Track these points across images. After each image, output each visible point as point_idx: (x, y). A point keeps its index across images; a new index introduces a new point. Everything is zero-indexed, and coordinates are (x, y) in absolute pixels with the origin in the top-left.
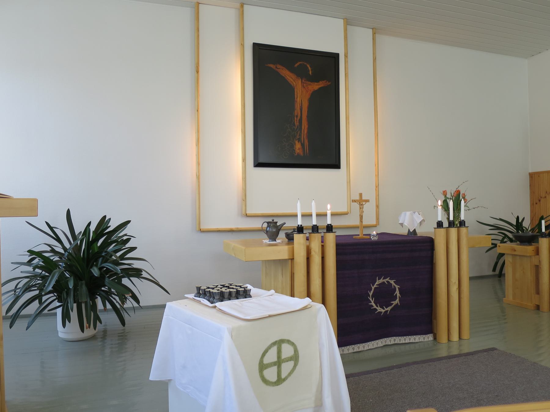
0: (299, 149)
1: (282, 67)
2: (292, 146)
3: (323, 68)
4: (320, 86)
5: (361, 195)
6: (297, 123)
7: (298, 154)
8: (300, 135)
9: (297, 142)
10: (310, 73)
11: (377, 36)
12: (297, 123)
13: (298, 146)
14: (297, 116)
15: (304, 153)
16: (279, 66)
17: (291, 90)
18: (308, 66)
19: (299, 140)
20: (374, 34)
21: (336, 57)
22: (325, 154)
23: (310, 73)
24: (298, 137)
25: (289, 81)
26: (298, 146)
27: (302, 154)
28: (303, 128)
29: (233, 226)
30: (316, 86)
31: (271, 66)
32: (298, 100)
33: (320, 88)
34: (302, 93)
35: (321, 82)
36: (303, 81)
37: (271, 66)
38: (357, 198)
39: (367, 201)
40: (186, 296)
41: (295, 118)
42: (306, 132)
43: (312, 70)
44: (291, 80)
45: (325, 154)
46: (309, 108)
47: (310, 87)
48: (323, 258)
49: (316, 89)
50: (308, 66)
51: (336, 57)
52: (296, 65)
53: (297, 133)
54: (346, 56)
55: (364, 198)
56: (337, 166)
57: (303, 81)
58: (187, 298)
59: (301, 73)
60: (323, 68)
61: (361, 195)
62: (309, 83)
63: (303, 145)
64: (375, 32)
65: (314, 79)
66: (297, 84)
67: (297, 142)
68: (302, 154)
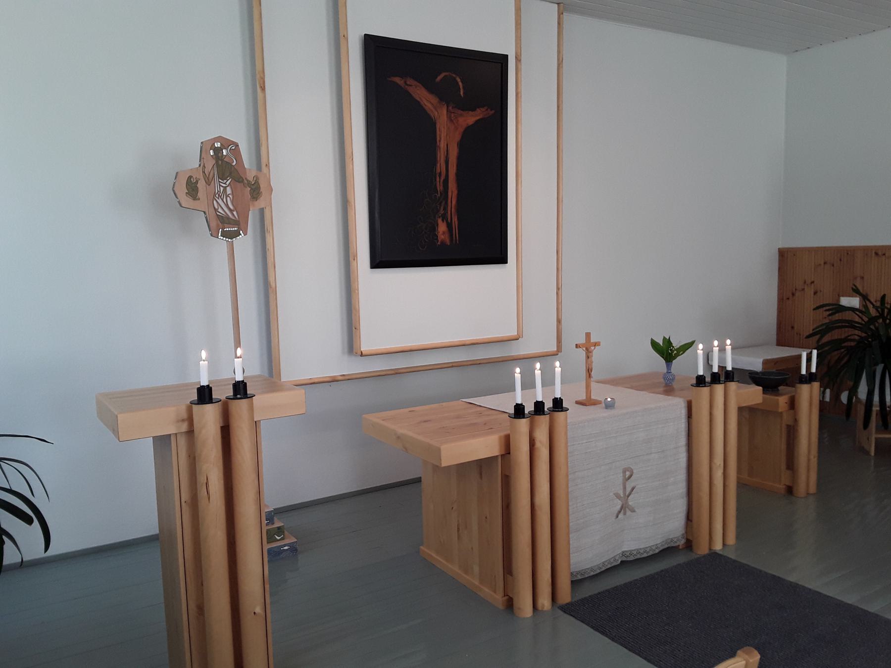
0: (444, 233)
1: (416, 83)
2: (434, 228)
3: (479, 81)
4: (478, 118)
5: (588, 335)
6: (440, 188)
7: (443, 243)
8: (445, 209)
9: (440, 221)
10: (462, 93)
11: (566, 16)
12: (440, 188)
13: (442, 227)
14: (440, 173)
15: (451, 240)
16: (410, 81)
17: (432, 125)
18: (458, 80)
19: (444, 218)
20: (560, 14)
21: (503, 60)
22: (481, 239)
23: (462, 93)
24: (442, 212)
25: (426, 108)
26: (442, 227)
27: (448, 242)
28: (450, 194)
29: (336, 373)
30: (470, 119)
31: (398, 80)
32: (442, 145)
33: (477, 122)
34: (449, 132)
35: (478, 111)
36: (450, 108)
37: (398, 80)
38: (582, 340)
39: (596, 344)
40: (828, 391)
41: (438, 179)
42: (454, 203)
43: (464, 88)
44: (429, 105)
45: (481, 239)
46: (459, 158)
47: (461, 120)
48: (711, 414)
49: (470, 123)
50: (458, 80)
51: (503, 60)
52: (439, 78)
53: (440, 204)
54: (518, 59)
55: (593, 340)
56: (502, 259)
57: (450, 108)
58: (824, 393)
59: (445, 94)
60: (479, 81)
61: (588, 335)
62: (460, 112)
63: (449, 226)
64: (563, 9)
65: (466, 105)
66: (441, 116)
67: (440, 221)
68: (448, 242)
